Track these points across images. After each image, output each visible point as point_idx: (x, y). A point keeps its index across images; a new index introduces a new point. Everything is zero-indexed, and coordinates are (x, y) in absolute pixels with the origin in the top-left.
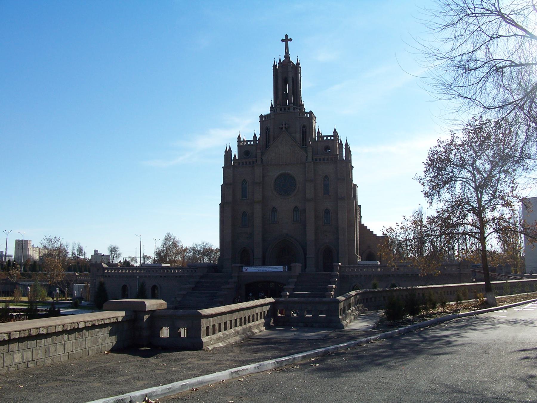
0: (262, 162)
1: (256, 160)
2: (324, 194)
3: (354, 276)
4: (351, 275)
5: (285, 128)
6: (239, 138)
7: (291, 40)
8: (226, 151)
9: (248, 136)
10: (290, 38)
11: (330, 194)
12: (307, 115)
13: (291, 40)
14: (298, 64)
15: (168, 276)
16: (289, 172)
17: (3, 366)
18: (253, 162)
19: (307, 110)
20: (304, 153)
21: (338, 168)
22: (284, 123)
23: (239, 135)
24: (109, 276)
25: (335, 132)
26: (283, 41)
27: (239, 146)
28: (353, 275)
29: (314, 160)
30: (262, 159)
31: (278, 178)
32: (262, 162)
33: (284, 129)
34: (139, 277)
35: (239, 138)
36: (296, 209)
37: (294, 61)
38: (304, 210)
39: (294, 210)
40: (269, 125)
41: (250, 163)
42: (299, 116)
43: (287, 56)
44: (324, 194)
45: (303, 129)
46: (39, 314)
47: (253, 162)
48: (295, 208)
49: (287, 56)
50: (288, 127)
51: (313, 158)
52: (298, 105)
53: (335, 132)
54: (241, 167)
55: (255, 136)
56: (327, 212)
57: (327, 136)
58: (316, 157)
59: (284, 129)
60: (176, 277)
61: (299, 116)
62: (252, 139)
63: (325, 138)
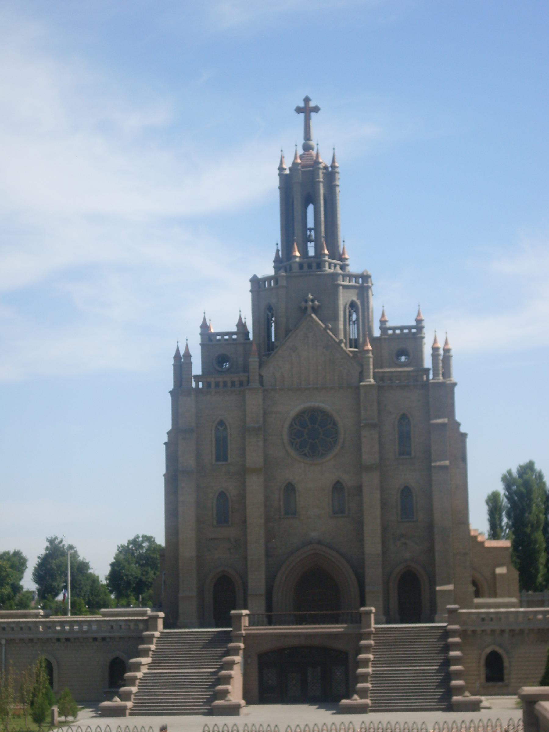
0: (261, 382)
1: (248, 377)
3: (469, 632)
6: (205, 327)
7: (316, 109)
8: (177, 357)
15: (75, 639)
16: (321, 405)
19: (353, 268)
24: (67, 640)
26: (299, 110)
31: (299, 418)
32: (261, 382)
34: (7, 641)
35: (205, 327)
36: (338, 487)
37: (325, 160)
38: (359, 489)
41: (233, 384)
43: (307, 148)
45: (268, 315)
46: (209, 706)
53: (419, 321)
55: (241, 325)
56: (406, 492)
60: (95, 639)
63: (390, 332)
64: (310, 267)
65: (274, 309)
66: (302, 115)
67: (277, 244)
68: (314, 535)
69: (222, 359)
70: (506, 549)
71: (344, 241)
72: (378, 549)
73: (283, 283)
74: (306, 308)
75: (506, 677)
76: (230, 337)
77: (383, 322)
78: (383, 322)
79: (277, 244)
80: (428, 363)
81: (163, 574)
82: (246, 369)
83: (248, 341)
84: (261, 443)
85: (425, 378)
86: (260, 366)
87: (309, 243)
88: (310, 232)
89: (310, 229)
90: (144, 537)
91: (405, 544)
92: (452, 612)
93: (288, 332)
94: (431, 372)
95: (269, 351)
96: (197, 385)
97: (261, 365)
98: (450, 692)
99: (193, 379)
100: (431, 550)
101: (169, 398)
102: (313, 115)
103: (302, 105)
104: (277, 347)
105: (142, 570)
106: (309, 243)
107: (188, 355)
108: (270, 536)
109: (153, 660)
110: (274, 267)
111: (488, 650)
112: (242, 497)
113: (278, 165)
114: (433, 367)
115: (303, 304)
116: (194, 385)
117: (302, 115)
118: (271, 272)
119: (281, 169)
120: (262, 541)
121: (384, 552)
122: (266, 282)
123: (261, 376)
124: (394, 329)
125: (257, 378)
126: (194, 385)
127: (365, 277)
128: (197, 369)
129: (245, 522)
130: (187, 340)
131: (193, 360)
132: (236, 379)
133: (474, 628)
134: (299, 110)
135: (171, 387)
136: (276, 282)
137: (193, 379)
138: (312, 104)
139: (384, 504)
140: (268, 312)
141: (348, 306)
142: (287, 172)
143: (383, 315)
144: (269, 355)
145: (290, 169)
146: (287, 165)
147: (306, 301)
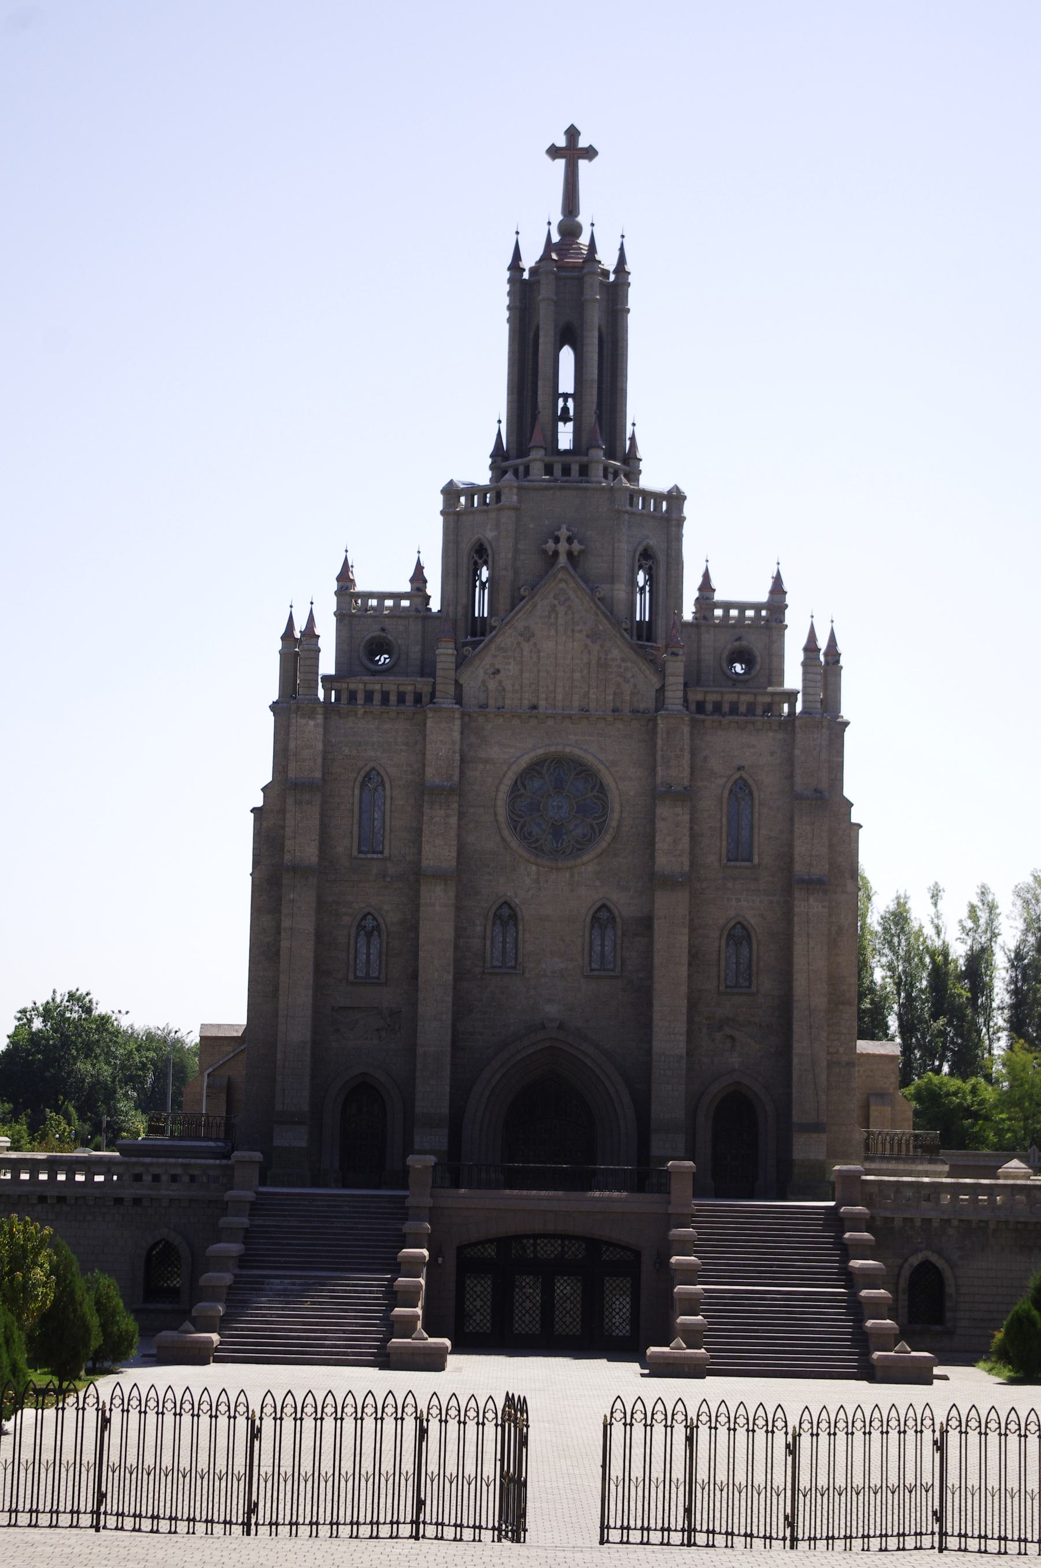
0: (459, 699)
2: (729, 860)
3: (918, 1223)
4: (923, 1220)
5: (570, 554)
6: (345, 578)
7: (590, 153)
8: (288, 636)
10: (586, 145)
11: (756, 860)
12: (658, 506)
13: (590, 153)
14: (621, 267)
17: (49, 1522)
18: (418, 699)
20: (648, 672)
21: (797, 752)
22: (564, 533)
24: (61, 1199)
25: (778, 588)
26: (554, 152)
27: (341, 616)
28: (911, 1220)
29: (693, 707)
30: (456, 682)
31: (534, 769)
32: (459, 699)
33: (563, 559)
35: (345, 578)
38: (646, 924)
39: (595, 918)
40: (490, 535)
42: (628, 508)
43: (570, 229)
44: (729, 860)
47: (418, 699)
48: (599, 910)
49: (570, 229)
50: (581, 552)
51: (686, 700)
52: (619, 455)
53: (778, 588)
54: (361, 712)
55: (419, 578)
57: (382, 596)
58: (700, 697)
59: (563, 559)
61: (628, 508)
62: (407, 588)
64: (566, 471)
65: (489, 552)
66: (561, 163)
67: (499, 422)
68: (552, 1010)
69: (378, 646)
70: (892, 1058)
71: (634, 424)
72: (681, 1047)
73: (510, 498)
74: (556, 553)
75: (949, 1315)
76: (397, 605)
77: (706, 587)
78: (706, 587)
79: (499, 422)
80: (793, 678)
81: (206, 1076)
82: (427, 669)
83: (429, 613)
84: (454, 820)
85: (786, 707)
86: (459, 665)
87: (561, 424)
88: (566, 401)
89: (566, 396)
90: (71, 996)
91: (732, 1038)
92: (852, 1178)
93: (516, 599)
94: (800, 696)
95: (476, 636)
96: (327, 696)
97: (461, 662)
98: (863, 1341)
99: (320, 684)
100: (785, 1051)
101: (269, 720)
102: (583, 164)
103: (561, 142)
104: (493, 628)
105: (1026, 1081)
106: (561, 424)
107: (310, 633)
108: (461, 1008)
109: (246, 1249)
110: (492, 467)
111: (915, 1260)
112: (412, 928)
113: (508, 260)
114: (805, 687)
115: (550, 545)
116: (321, 694)
117: (561, 163)
118: (483, 477)
119: (515, 265)
120: (447, 1018)
121: (690, 1053)
122: (476, 497)
123: (458, 685)
124: (727, 606)
125: (451, 689)
126: (321, 694)
127: (676, 498)
128: (327, 665)
129: (415, 976)
130: (707, 561)
131: (321, 643)
132: (392, 688)
133: (888, 1214)
134: (554, 152)
135: (273, 694)
136: (498, 497)
137: (320, 684)
138: (583, 143)
139: (694, 956)
140: (476, 558)
141: (638, 554)
142: (526, 275)
143: (706, 576)
144: (475, 645)
145: (533, 271)
146: (529, 261)
147: (557, 540)
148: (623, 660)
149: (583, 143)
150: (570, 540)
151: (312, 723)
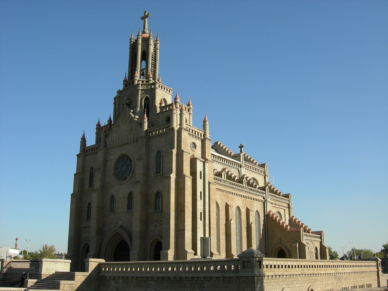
9: (104, 122)
23: (99, 120)
33: (125, 105)
55: (110, 121)
59: (125, 105)
74: (124, 104)
123: (106, 143)
148: (136, 126)
149: (143, 15)
150: (126, 100)
151: (80, 159)
